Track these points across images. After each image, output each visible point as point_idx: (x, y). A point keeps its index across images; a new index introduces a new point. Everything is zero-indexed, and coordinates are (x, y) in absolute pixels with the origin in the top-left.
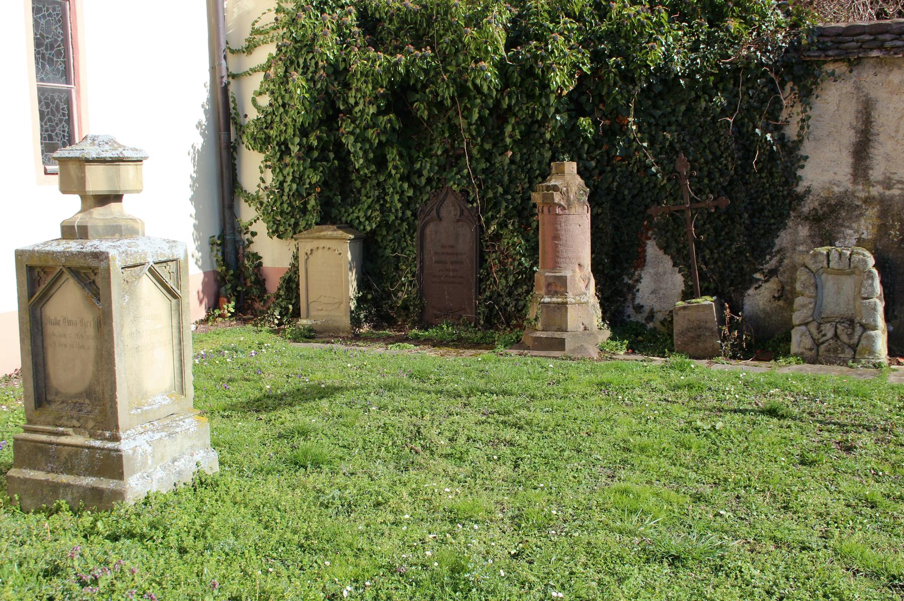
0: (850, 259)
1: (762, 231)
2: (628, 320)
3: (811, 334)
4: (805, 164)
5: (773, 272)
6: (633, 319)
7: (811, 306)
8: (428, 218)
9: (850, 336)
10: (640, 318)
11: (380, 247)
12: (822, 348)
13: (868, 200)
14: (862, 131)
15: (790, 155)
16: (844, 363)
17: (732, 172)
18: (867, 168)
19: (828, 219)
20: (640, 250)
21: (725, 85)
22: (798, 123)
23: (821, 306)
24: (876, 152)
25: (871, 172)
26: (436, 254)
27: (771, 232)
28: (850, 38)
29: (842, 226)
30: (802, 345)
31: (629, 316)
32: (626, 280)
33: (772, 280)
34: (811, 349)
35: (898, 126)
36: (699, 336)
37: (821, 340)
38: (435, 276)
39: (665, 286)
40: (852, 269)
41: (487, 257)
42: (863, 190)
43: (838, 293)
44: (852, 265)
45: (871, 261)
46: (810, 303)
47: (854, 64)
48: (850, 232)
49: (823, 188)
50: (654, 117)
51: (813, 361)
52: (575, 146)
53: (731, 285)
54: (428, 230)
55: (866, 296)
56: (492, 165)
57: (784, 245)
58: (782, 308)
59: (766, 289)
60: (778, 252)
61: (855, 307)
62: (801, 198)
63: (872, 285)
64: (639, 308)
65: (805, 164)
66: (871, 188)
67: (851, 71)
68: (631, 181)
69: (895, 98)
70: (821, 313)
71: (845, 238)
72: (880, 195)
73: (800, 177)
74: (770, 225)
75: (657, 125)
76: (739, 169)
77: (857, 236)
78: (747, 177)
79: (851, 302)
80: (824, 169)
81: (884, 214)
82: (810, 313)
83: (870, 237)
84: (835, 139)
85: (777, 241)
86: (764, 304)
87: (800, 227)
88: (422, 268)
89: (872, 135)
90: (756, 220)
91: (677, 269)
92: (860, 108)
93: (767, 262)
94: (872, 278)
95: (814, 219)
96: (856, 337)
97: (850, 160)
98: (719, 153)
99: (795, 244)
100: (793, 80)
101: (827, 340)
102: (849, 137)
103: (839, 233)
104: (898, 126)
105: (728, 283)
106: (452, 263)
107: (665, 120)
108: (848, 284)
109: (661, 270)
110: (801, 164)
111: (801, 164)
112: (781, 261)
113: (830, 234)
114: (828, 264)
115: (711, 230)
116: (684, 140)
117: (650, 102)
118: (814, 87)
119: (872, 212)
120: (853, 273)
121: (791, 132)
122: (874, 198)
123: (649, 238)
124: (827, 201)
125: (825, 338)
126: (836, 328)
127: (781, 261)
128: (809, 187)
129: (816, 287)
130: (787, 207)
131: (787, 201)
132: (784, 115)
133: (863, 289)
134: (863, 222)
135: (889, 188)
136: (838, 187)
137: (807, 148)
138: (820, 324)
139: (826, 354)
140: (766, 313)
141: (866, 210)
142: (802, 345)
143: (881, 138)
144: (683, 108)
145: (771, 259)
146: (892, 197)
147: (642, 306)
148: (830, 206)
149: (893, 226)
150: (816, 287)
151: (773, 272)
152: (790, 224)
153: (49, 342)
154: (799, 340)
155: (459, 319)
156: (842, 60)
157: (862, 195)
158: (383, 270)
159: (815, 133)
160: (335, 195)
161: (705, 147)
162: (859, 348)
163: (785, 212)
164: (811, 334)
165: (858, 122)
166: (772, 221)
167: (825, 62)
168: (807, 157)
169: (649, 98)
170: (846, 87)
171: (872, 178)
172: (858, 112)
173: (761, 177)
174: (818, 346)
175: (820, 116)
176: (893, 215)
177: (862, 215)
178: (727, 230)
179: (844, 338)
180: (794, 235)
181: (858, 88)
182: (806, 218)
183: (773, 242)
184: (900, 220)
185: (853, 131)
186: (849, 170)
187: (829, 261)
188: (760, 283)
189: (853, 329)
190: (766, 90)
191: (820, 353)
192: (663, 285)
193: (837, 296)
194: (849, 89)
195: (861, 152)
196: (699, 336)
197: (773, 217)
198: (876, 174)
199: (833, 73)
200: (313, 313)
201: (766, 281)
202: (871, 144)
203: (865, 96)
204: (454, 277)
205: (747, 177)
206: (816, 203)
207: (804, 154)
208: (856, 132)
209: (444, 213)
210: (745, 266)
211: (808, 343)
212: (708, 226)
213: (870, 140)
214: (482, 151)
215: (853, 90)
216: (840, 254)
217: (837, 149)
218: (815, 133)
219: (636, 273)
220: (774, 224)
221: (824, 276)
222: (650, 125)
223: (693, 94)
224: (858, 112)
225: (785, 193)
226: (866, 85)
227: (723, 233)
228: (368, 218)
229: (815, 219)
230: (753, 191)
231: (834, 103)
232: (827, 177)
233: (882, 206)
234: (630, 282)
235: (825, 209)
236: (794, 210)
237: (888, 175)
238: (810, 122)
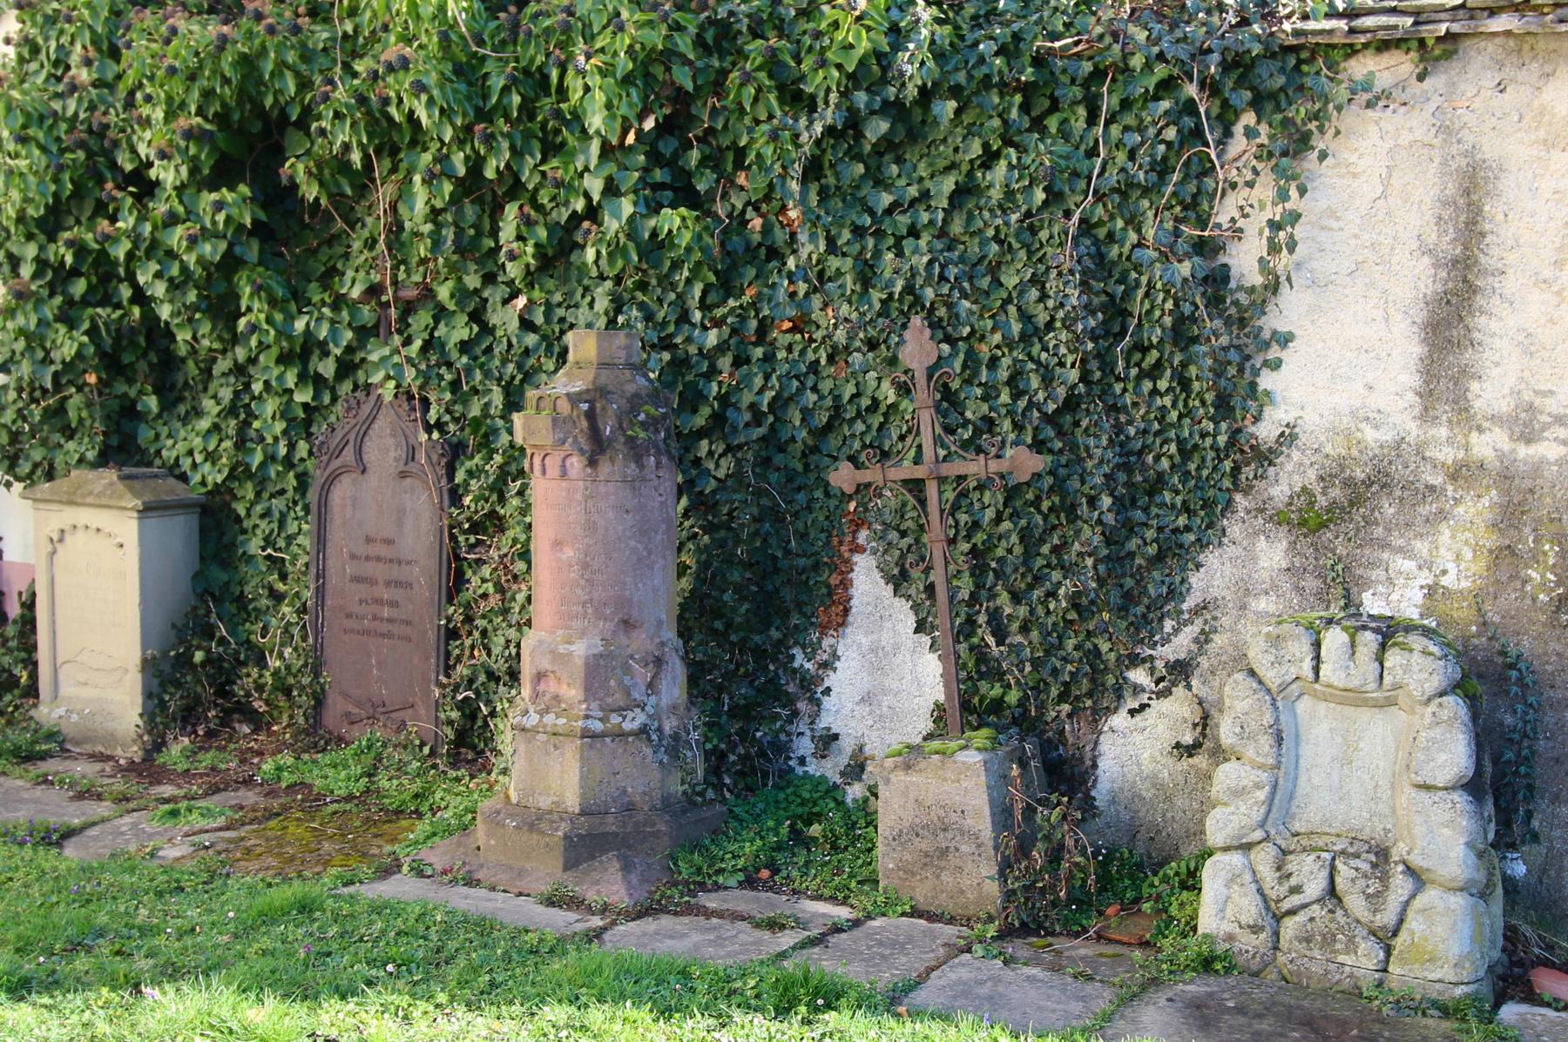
1: (1152, 550)
2: (800, 770)
4: (1284, 355)
5: (1181, 670)
6: (811, 769)
7: (1261, 795)
8: (336, 463)
9: (1375, 900)
10: (829, 769)
11: (244, 532)
12: (1290, 927)
13: (1464, 473)
14: (1455, 262)
15: (1222, 333)
17: (1074, 375)
20: (834, 580)
21: (1065, 121)
22: (1261, 233)
24: (1494, 325)
25: (1474, 386)
26: (353, 557)
27: (1176, 553)
29: (1384, 545)
31: (802, 761)
32: (799, 659)
33: (1179, 691)
34: (1255, 929)
36: (944, 853)
37: (1286, 905)
38: (349, 616)
39: (895, 685)
41: (469, 574)
42: (1449, 441)
44: (1387, 679)
48: (1408, 565)
49: (1333, 431)
50: (872, 213)
52: (673, 286)
53: (1062, 698)
54: (339, 493)
56: (487, 330)
57: (1215, 592)
59: (1161, 715)
62: (1265, 457)
64: (829, 740)
65: (1284, 355)
66: (1474, 435)
68: (814, 389)
71: (1390, 582)
72: (1501, 456)
73: (1267, 393)
74: (1176, 531)
75: (879, 234)
76: (1094, 365)
77: (1425, 578)
78: (1118, 387)
80: (1335, 373)
81: (1510, 515)
82: (1257, 815)
83: (1465, 584)
85: (1196, 579)
86: (1154, 760)
88: (320, 592)
89: (1485, 273)
90: (1138, 515)
91: (926, 640)
92: (1451, 189)
93: (1166, 641)
95: (1303, 523)
97: (1417, 350)
98: (1042, 318)
99: (1246, 591)
100: (1256, 104)
101: (1305, 906)
102: (1415, 280)
103: (1372, 565)
105: (1054, 692)
106: (388, 584)
107: (903, 220)
109: (886, 639)
112: (1203, 639)
114: (1316, 670)
115: (1014, 538)
116: (943, 278)
117: (860, 169)
118: (1313, 126)
120: (1390, 702)
121: (1244, 261)
123: (860, 549)
124: (1342, 468)
125: (1296, 900)
127: (1203, 639)
129: (1279, 740)
130: (1227, 483)
131: (1227, 465)
132: (1225, 212)
134: (1445, 536)
136: (1377, 427)
137: (1287, 312)
139: (1302, 947)
140: (1158, 786)
142: (1229, 913)
143: (1511, 284)
144: (948, 184)
145: (1176, 631)
146: (1537, 468)
147: (836, 737)
148: (1348, 483)
149: (1536, 557)
150: (1279, 740)
151: (1181, 670)
155: (399, 731)
157: (1447, 455)
158: (247, 589)
159: (1314, 264)
160: (141, 393)
161: (1009, 301)
162: (1399, 942)
168: (1285, 340)
169: (859, 157)
171: (1477, 404)
172: (1445, 204)
173: (1155, 392)
174: (1278, 918)
175: (1332, 214)
176: (1539, 521)
177: (1442, 515)
178: (1056, 541)
179: (1356, 904)
181: (1445, 131)
182: (1279, 519)
184: (1557, 539)
185: (1426, 260)
188: (1144, 698)
189: (1384, 879)
190: (1171, 134)
191: (1283, 944)
192: (891, 683)
194: (1419, 134)
195: (1450, 321)
196: (944, 853)
198: (1492, 392)
199: (1367, 86)
200: (66, 690)
201: (1162, 694)
202: (1479, 300)
203: (1466, 154)
204: (390, 620)
205: (1118, 387)
206: (1312, 475)
207: (1283, 328)
208: (1436, 266)
209: (371, 453)
210: (1105, 647)
212: (1006, 525)
214: (461, 294)
215: (1429, 138)
217: (1379, 314)
218: (1314, 264)
219: (826, 643)
220: (1188, 529)
222: (859, 232)
223: (976, 149)
224: (1445, 204)
225: (1222, 440)
226: (1468, 117)
227: (1045, 549)
228: (211, 457)
229: (1307, 521)
230: (1132, 431)
234: (808, 665)
235: (1336, 492)
236: (1246, 492)
237: (1527, 396)
238: (1299, 231)
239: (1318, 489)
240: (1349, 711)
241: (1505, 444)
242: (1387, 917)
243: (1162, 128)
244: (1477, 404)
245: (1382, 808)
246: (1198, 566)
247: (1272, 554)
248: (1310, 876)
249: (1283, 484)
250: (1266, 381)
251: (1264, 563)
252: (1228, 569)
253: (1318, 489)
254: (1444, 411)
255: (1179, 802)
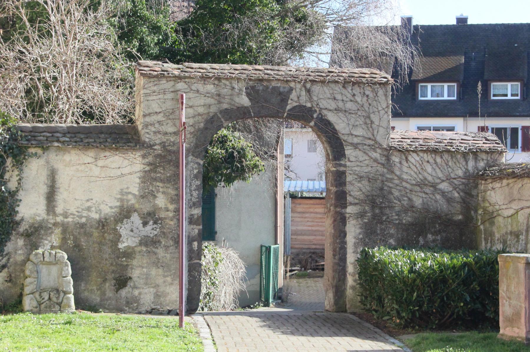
0: (55, 256)
3: (36, 299)
7: (36, 283)
9: (58, 298)
12: (43, 306)
13: (55, 224)
16: (56, 312)
18: (54, 206)
19: (34, 235)
23: (40, 283)
24: (58, 198)
25: (56, 209)
28: (39, 134)
29: (42, 239)
30: (31, 305)
33: (3, 271)
34: (36, 307)
35: (69, 184)
37: (42, 302)
40: (56, 262)
42: (53, 219)
43: (49, 275)
44: (57, 259)
45: (66, 257)
46: (35, 281)
47: (45, 149)
48: (46, 242)
49: (31, 218)
51: (40, 312)
55: (65, 275)
57: (10, 251)
58: (10, 287)
60: (7, 254)
61: (58, 282)
62: (18, 223)
63: (68, 270)
66: (57, 218)
67: (44, 153)
69: (67, 169)
70: (40, 287)
71: (44, 245)
72: (62, 221)
73: (17, 211)
77: (50, 244)
79: (57, 280)
80: (30, 207)
82: (35, 287)
83: (57, 245)
84: (36, 190)
85: (5, 248)
87: (19, 240)
89: (56, 188)
92: (49, 173)
94: (68, 266)
95: (26, 235)
96: (61, 299)
99: (16, 250)
102: (44, 189)
103: (40, 243)
104: (69, 184)
108: (54, 270)
110: (17, 204)
111: (17, 204)
112: (9, 259)
113: (36, 244)
114: (44, 259)
118: (24, 161)
119: (58, 231)
120: (57, 263)
122: (58, 223)
125: (44, 301)
126: (50, 294)
127: (9, 259)
128: (23, 217)
129: (38, 272)
130: (11, 229)
131: (11, 225)
133: (63, 273)
134: (53, 236)
135: (66, 217)
137: (21, 195)
138: (41, 293)
141: (55, 230)
143: (61, 190)
146: (68, 223)
148: (35, 227)
149: (69, 239)
150: (38, 272)
152: (13, 238)
153: (218, 202)
154: (28, 302)
156: (39, 147)
157: (52, 221)
163: (10, 232)
164: (36, 299)
165: (48, 181)
166: (3, 237)
167: (29, 147)
168: (21, 200)
170: (41, 162)
174: (40, 305)
175: (27, 177)
176: (69, 233)
177: (52, 232)
179: (54, 299)
180: (16, 245)
181: (48, 162)
182: (22, 235)
183: (3, 249)
185: (46, 186)
186: (44, 208)
187: (44, 258)
189: (59, 294)
191: (42, 309)
193: (49, 276)
194: (43, 163)
197: (3, 234)
198: (59, 210)
202: (56, 193)
206: (27, 226)
208: (48, 187)
211: (35, 304)
213: (55, 191)
216: (50, 253)
221: (41, 266)
225: (10, 220)
226: (52, 161)
229: (27, 235)
231: (35, 169)
232: (32, 211)
233: (63, 227)
235: (32, 229)
236: (15, 230)
239: (29, 229)
240: (49, 266)
241: (62, 219)
242: (60, 300)
243: (428, 173)
244: (57, 212)
245: (56, 282)
246: (6, 246)
247: (21, 242)
248: (46, 296)
249: (21, 229)
250: (17, 209)
251: (19, 244)
252: (12, 246)
253: (29, 229)
254: (51, 213)
255: (5, 293)
